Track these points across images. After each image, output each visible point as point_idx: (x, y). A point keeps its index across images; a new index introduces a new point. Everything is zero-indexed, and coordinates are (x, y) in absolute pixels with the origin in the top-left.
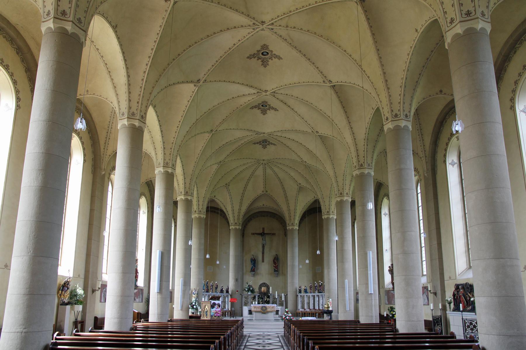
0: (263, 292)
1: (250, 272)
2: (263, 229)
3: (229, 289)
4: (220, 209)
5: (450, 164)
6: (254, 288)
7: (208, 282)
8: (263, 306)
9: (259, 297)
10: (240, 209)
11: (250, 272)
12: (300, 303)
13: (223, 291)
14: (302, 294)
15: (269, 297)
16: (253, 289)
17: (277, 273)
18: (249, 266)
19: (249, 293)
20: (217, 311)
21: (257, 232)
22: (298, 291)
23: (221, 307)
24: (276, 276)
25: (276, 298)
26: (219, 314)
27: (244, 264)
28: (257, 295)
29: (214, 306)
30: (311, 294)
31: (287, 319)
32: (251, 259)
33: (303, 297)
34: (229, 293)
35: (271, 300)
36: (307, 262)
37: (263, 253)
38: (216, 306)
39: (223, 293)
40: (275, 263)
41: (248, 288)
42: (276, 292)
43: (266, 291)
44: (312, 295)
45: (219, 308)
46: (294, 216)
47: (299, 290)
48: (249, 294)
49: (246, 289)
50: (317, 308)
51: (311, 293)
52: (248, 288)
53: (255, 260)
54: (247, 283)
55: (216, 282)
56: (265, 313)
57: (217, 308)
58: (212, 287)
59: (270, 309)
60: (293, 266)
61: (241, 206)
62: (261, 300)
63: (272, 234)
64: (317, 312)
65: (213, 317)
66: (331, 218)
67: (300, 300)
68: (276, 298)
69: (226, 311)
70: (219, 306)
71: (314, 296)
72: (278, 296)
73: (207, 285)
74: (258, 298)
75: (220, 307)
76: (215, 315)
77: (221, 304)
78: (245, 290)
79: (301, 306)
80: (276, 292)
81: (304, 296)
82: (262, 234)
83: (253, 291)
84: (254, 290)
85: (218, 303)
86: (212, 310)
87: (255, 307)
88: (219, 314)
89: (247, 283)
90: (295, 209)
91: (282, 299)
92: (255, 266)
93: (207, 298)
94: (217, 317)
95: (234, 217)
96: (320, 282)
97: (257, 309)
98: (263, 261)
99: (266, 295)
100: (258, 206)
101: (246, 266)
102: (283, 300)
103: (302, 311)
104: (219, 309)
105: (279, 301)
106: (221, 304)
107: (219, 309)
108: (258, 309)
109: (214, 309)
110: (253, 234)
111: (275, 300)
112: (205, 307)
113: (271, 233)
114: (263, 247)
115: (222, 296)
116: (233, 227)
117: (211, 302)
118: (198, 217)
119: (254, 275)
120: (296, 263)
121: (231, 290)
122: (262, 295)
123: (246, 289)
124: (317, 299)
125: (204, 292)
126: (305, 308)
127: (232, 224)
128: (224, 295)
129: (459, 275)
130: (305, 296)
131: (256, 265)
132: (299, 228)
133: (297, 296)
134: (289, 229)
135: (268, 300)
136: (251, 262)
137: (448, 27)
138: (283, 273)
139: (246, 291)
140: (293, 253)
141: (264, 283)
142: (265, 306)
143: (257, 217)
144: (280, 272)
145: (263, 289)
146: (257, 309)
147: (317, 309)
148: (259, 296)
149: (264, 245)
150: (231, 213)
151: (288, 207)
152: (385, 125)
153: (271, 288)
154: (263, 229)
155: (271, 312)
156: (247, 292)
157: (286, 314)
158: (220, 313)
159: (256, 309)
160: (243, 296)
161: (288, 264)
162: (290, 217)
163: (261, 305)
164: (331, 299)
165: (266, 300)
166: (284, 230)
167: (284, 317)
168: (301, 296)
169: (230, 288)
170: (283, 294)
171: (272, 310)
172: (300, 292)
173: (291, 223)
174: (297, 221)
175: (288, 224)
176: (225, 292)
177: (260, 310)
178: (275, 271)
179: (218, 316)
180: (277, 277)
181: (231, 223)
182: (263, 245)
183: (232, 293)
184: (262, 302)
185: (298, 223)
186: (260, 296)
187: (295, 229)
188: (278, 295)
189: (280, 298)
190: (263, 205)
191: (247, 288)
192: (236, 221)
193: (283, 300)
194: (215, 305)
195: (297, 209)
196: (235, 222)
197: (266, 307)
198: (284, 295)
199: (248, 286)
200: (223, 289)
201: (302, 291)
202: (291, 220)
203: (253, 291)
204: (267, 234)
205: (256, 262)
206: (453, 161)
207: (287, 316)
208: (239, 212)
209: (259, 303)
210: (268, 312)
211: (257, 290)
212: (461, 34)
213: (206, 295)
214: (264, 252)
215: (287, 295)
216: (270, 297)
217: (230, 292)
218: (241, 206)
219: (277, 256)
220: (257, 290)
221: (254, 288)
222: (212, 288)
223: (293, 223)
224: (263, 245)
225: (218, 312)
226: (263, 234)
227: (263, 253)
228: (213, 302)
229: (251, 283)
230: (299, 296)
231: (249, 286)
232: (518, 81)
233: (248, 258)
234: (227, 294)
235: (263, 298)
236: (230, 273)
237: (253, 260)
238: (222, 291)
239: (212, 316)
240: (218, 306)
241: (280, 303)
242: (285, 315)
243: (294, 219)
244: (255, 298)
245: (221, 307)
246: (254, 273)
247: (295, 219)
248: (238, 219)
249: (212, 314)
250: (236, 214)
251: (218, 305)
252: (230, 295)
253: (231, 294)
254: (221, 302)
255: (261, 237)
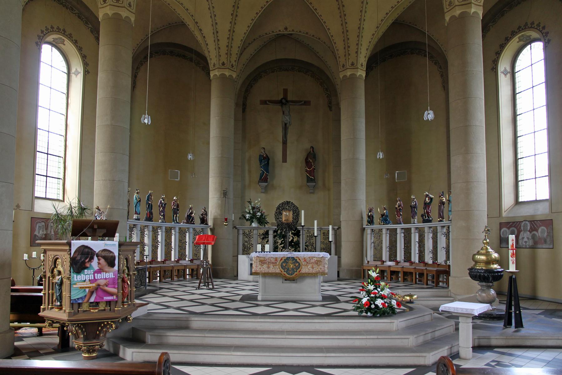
0: (285, 222)
1: (259, 182)
2: (285, 91)
3: (206, 214)
4: (195, 50)
5: (502, 72)
6: (266, 214)
7: (150, 195)
8: (288, 258)
9: (276, 234)
10: (232, 31)
11: (259, 182)
12: (371, 248)
13: (193, 219)
14: (376, 226)
15: (297, 234)
16: (262, 215)
17: (314, 184)
18: (256, 170)
19: (254, 225)
20: (102, 282)
21: (274, 99)
22: (365, 219)
23: (116, 268)
24: (312, 191)
25: (316, 235)
26: (111, 294)
27: (247, 168)
28: (271, 227)
29: (84, 263)
30: (399, 227)
31: (377, 306)
32: (260, 156)
33: (378, 234)
34: (207, 224)
35: (302, 240)
36: (381, 155)
37: (285, 143)
38: (95, 263)
39: (194, 224)
40: (308, 163)
41: (251, 212)
42: (316, 222)
43: (291, 219)
44: (402, 229)
45: (107, 268)
46: (357, 44)
47: (369, 217)
48: (254, 228)
49: (248, 216)
50: (428, 259)
51: (401, 224)
52: (251, 212)
53: (269, 159)
54: (250, 202)
55: (174, 198)
56: (293, 280)
57: (100, 271)
58: (164, 208)
59: (310, 266)
60: (354, 161)
61: (233, 23)
62: (280, 241)
63: (303, 102)
64: (430, 271)
65: (85, 307)
66: (473, 13)
67: (369, 239)
68: (316, 235)
69: (186, 267)
70: (111, 262)
71: (407, 232)
72: (319, 232)
73: (147, 203)
74: (275, 237)
75: (112, 264)
76: (92, 300)
77: (116, 254)
78: (245, 217)
79: (372, 254)
80: (316, 222)
81: (381, 230)
82: (284, 101)
83: (262, 221)
84: (264, 219)
85: (105, 250)
86: (76, 278)
87: (262, 262)
88: (111, 294)
89: (250, 202)
90: (359, 28)
91: (328, 238)
92: (267, 171)
93: (149, 236)
94: (102, 307)
95: (219, 48)
96: (427, 196)
97: (269, 267)
98: (285, 160)
99: (291, 229)
100: (273, 32)
101: (250, 172)
102: (330, 240)
103: (390, 267)
104: (110, 274)
105: (322, 243)
106: (116, 254)
107: (110, 274)
108: (271, 266)
109: (87, 275)
110: (264, 102)
111: (312, 241)
112: (55, 267)
113: (302, 101)
114: (285, 128)
115: (191, 230)
116: (217, 73)
117: (69, 244)
118: (110, 15)
119: (266, 190)
120: (362, 155)
121: (212, 217)
122: (282, 230)
123: (248, 216)
124: (415, 238)
125: (138, 219)
126: (384, 259)
127: (214, 65)
128: (194, 229)
129: (505, 212)
130: (384, 231)
131: (270, 168)
132: (366, 73)
133: (363, 230)
134: (345, 76)
135: (295, 240)
136: (261, 161)
137: (447, 9)
138: (324, 184)
139: (247, 220)
140: (354, 130)
141: (288, 203)
142: (293, 258)
143: (273, 72)
144: (320, 183)
145: (287, 216)
146: (269, 267)
147: (430, 262)
148: (275, 231)
149: (288, 125)
150: (213, 39)
151: (344, 24)
152: (446, 13)
153: (303, 212)
154: (285, 91)
155: (313, 275)
156: (249, 222)
157: (371, 287)
158: (114, 290)
159: (265, 266)
160: (241, 232)
161: (342, 159)
162: (347, 47)
163: (280, 254)
164: (35, 252)
165: (292, 240)
166: (327, 97)
167: (364, 300)
168: (372, 229)
169: (211, 212)
170: (330, 227)
171: (316, 269)
172: (371, 221)
173: (350, 63)
174: (363, 60)
175: (343, 66)
176: (197, 220)
177: (277, 270)
178: (309, 180)
179: (109, 303)
180: (313, 193)
181: (212, 65)
182: (286, 124)
183: (214, 225)
184: (282, 245)
185: (365, 64)
186: (279, 231)
187: (360, 75)
188: (319, 229)
189: (322, 234)
190: (286, 29)
191: (249, 213)
192: (223, 59)
193: (330, 240)
194: (92, 259)
195: (363, 28)
196: (221, 62)
197: (296, 262)
198: (333, 229)
199: (250, 208)
200: (191, 213)
201: (377, 219)
202: (349, 54)
203: (262, 221)
204: (293, 102)
205: (270, 162)
206: (505, 69)
207: (376, 298)
208: (231, 39)
209: (275, 249)
210: (304, 276)
211: (271, 219)
212: (456, 17)
213: (145, 226)
214: (287, 141)
215: (339, 228)
216: (301, 233)
217: (210, 223)
218: (235, 24)
219: (313, 151)
220: (271, 219)
221: (266, 214)
222: (163, 211)
223: (355, 63)
224: (286, 124)
225: (107, 285)
226: (283, 102)
227: (285, 143)
228: (77, 244)
229: (257, 202)
230: (369, 231)
231: (253, 208)
232: (504, 44)
233: (253, 154)
234: (203, 226)
235: (284, 237)
236: (210, 179)
237: (264, 158)
238: (190, 219)
239: (73, 303)
240: (102, 261)
241: (323, 246)
242: (369, 292)
243: (357, 52)
244: (268, 235)
245: (116, 268)
246: (266, 184)
247: (359, 53)
248: (229, 54)
249: (76, 295)
250: (224, 43)
251: (105, 258)
252: (210, 229)
253: (212, 227)
254: (117, 244)
255: (280, 107)
